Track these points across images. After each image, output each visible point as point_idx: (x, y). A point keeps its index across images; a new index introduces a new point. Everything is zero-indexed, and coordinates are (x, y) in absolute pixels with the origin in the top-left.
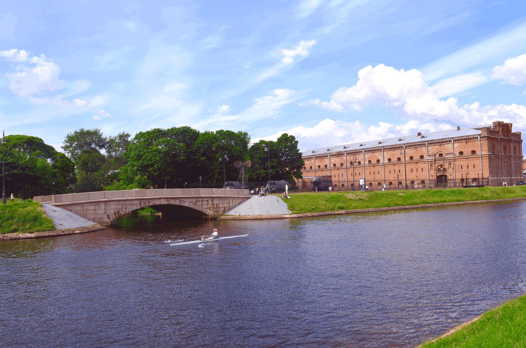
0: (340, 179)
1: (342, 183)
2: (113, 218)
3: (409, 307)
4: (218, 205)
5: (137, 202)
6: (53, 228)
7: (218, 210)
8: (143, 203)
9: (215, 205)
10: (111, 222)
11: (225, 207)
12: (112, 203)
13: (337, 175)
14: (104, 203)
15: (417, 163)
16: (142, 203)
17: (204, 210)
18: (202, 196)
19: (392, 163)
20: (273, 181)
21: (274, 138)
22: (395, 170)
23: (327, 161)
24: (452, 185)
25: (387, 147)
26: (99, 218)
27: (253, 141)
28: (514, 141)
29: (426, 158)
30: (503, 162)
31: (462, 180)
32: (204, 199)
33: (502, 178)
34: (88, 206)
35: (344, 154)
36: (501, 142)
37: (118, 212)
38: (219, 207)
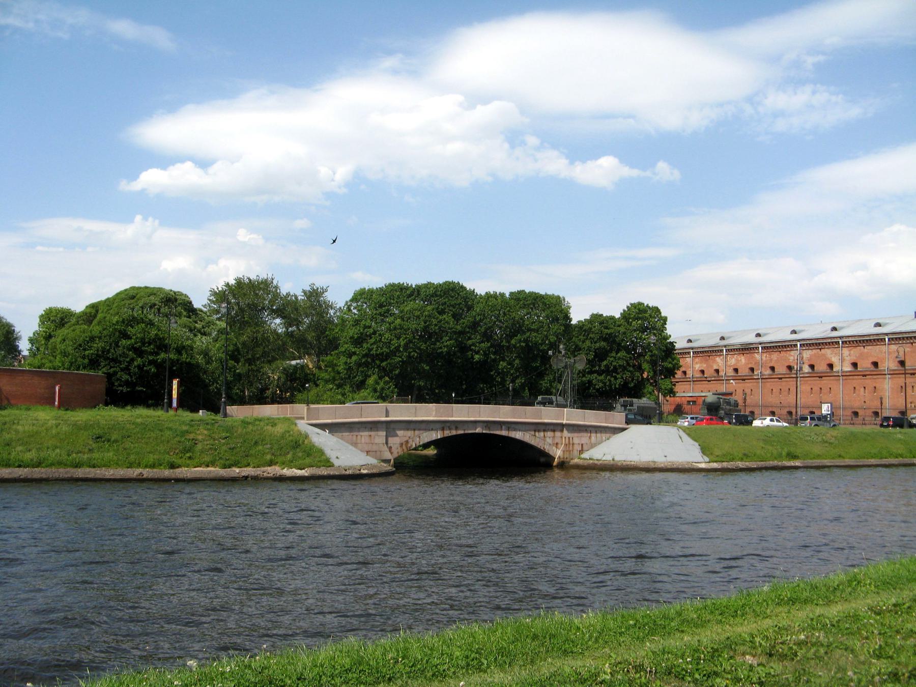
1: (788, 410)
2: (398, 453)
3: (480, 602)
4: (571, 439)
6: (328, 463)
18: (546, 421)
19: (860, 371)
21: (614, 309)
22: (865, 388)
27: (577, 316)
32: (548, 427)
35: (757, 348)
37: (407, 442)
38: (573, 444)
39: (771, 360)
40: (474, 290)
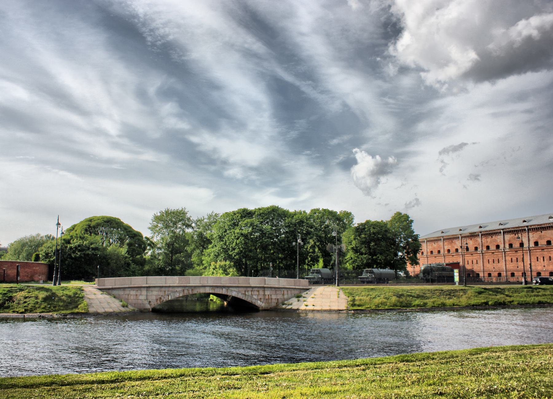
0: (474, 267)
4: (270, 296)
5: (180, 289)
8: (187, 291)
9: (267, 296)
11: (278, 299)
12: (153, 289)
13: (470, 262)
14: (146, 289)
16: (185, 290)
17: (254, 301)
19: (540, 247)
20: (370, 269)
22: (543, 257)
25: (533, 227)
26: (140, 304)
34: (129, 291)
37: (160, 298)
39: (487, 242)
40: (295, 211)
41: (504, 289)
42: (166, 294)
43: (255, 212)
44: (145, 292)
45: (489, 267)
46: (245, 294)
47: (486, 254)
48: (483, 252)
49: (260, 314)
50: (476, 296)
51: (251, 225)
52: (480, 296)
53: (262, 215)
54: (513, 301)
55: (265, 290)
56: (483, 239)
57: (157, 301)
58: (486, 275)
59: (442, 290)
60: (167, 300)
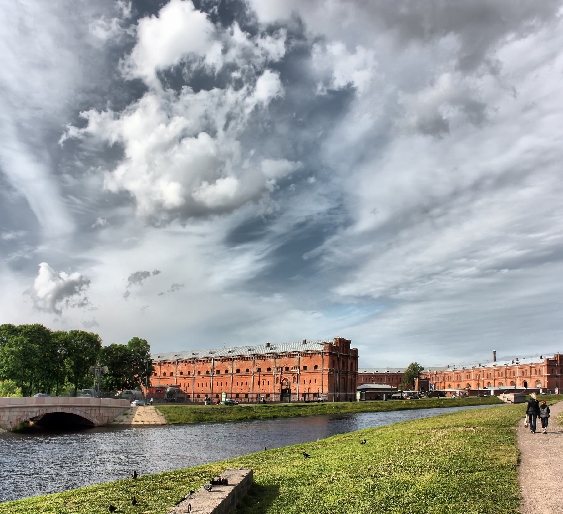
5: (36, 409)
7: (103, 419)
9: (102, 414)
10: (13, 429)
15: (264, 375)
19: (241, 374)
21: (124, 341)
22: (242, 382)
23: (173, 368)
24: (295, 399)
27: (104, 344)
28: (352, 357)
29: (274, 370)
30: (341, 378)
31: (304, 395)
33: (338, 393)
36: (340, 357)
37: (20, 418)
38: (104, 417)
41: (252, 407)
42: (25, 414)
43: (22, 329)
44: (8, 412)
45: (199, 390)
46: (86, 413)
47: (197, 378)
48: (195, 376)
49: (95, 429)
50: (239, 413)
51: (21, 343)
52: (241, 412)
53: (29, 333)
54: (260, 416)
55: (100, 409)
56: (196, 365)
57: (17, 421)
58: (195, 396)
59: (217, 408)
60: (26, 420)
